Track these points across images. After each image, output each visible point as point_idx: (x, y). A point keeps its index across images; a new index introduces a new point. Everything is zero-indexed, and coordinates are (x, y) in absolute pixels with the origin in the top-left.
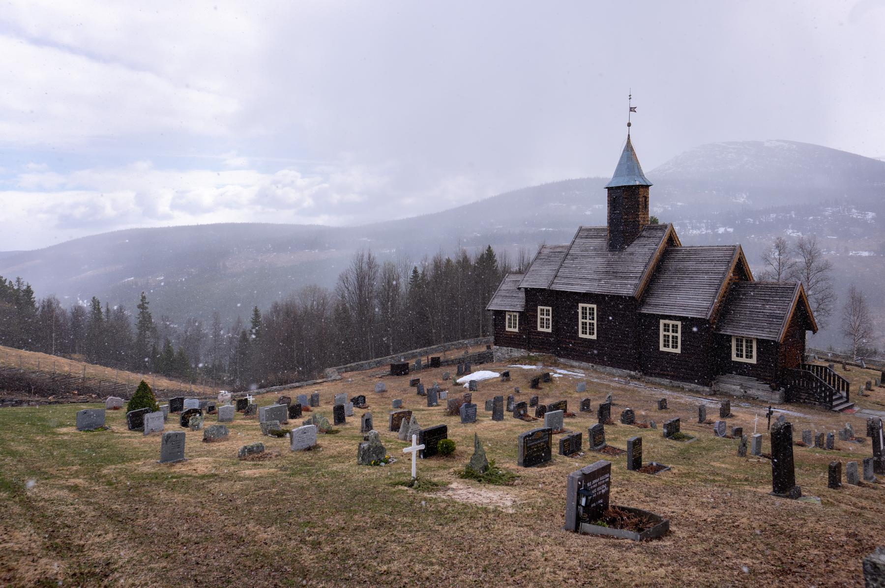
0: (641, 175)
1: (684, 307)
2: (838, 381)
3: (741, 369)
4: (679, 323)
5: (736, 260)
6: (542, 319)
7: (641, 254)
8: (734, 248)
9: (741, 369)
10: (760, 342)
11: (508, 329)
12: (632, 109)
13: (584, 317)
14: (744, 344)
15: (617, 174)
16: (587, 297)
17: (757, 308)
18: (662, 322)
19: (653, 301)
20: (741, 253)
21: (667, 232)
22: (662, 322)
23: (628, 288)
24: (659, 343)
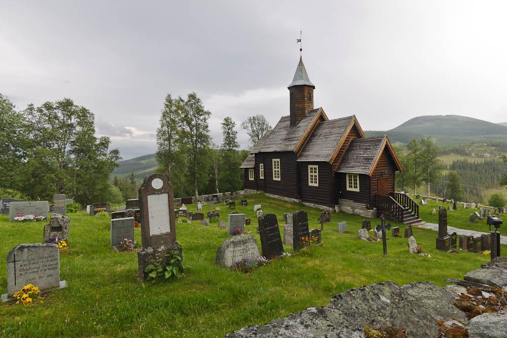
0: (308, 80)
1: (318, 156)
2: (410, 201)
3: (353, 196)
4: (317, 166)
5: (352, 125)
6: (312, 176)
7: (305, 126)
8: (350, 118)
9: (353, 196)
10: (360, 175)
11: (310, 184)
12: (300, 41)
13: (311, 172)
14: (353, 177)
15: (295, 79)
16: (275, 154)
17: (360, 154)
18: (310, 166)
19: (306, 153)
20: (356, 121)
21: (319, 112)
22: (310, 166)
23: (293, 147)
24: (360, 184)
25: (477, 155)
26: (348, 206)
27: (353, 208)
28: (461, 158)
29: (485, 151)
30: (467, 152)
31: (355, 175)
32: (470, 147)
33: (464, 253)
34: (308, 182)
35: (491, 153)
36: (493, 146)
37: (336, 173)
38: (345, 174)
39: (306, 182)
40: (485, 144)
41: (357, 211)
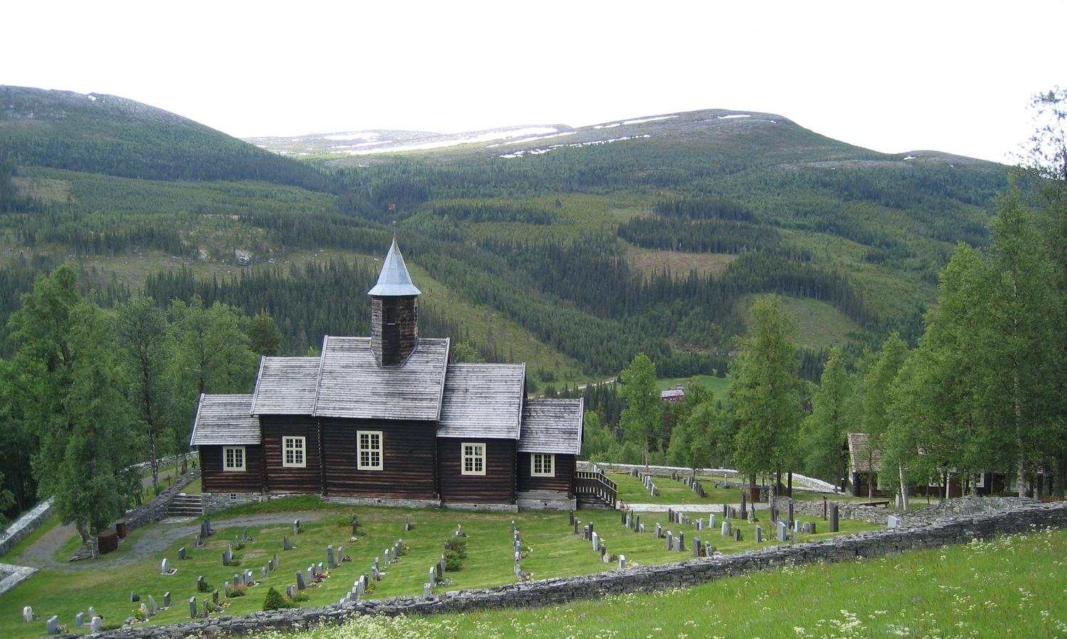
4: (484, 446)
10: (558, 456)
18: (464, 445)
25: (215, 254)
26: (534, 500)
27: (545, 501)
28: (170, 265)
29: (239, 243)
30: (186, 243)
31: (548, 456)
32: (191, 228)
33: (609, 597)
34: (282, 462)
35: (255, 248)
36: (258, 223)
37: (518, 452)
38: (529, 454)
39: (310, 459)
40: (236, 217)
41: (552, 504)
